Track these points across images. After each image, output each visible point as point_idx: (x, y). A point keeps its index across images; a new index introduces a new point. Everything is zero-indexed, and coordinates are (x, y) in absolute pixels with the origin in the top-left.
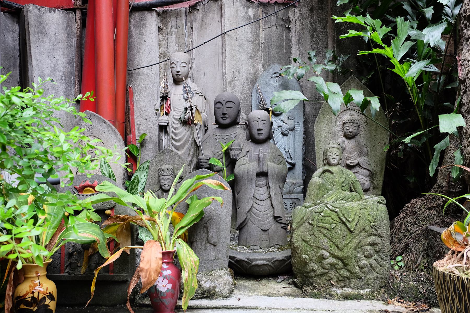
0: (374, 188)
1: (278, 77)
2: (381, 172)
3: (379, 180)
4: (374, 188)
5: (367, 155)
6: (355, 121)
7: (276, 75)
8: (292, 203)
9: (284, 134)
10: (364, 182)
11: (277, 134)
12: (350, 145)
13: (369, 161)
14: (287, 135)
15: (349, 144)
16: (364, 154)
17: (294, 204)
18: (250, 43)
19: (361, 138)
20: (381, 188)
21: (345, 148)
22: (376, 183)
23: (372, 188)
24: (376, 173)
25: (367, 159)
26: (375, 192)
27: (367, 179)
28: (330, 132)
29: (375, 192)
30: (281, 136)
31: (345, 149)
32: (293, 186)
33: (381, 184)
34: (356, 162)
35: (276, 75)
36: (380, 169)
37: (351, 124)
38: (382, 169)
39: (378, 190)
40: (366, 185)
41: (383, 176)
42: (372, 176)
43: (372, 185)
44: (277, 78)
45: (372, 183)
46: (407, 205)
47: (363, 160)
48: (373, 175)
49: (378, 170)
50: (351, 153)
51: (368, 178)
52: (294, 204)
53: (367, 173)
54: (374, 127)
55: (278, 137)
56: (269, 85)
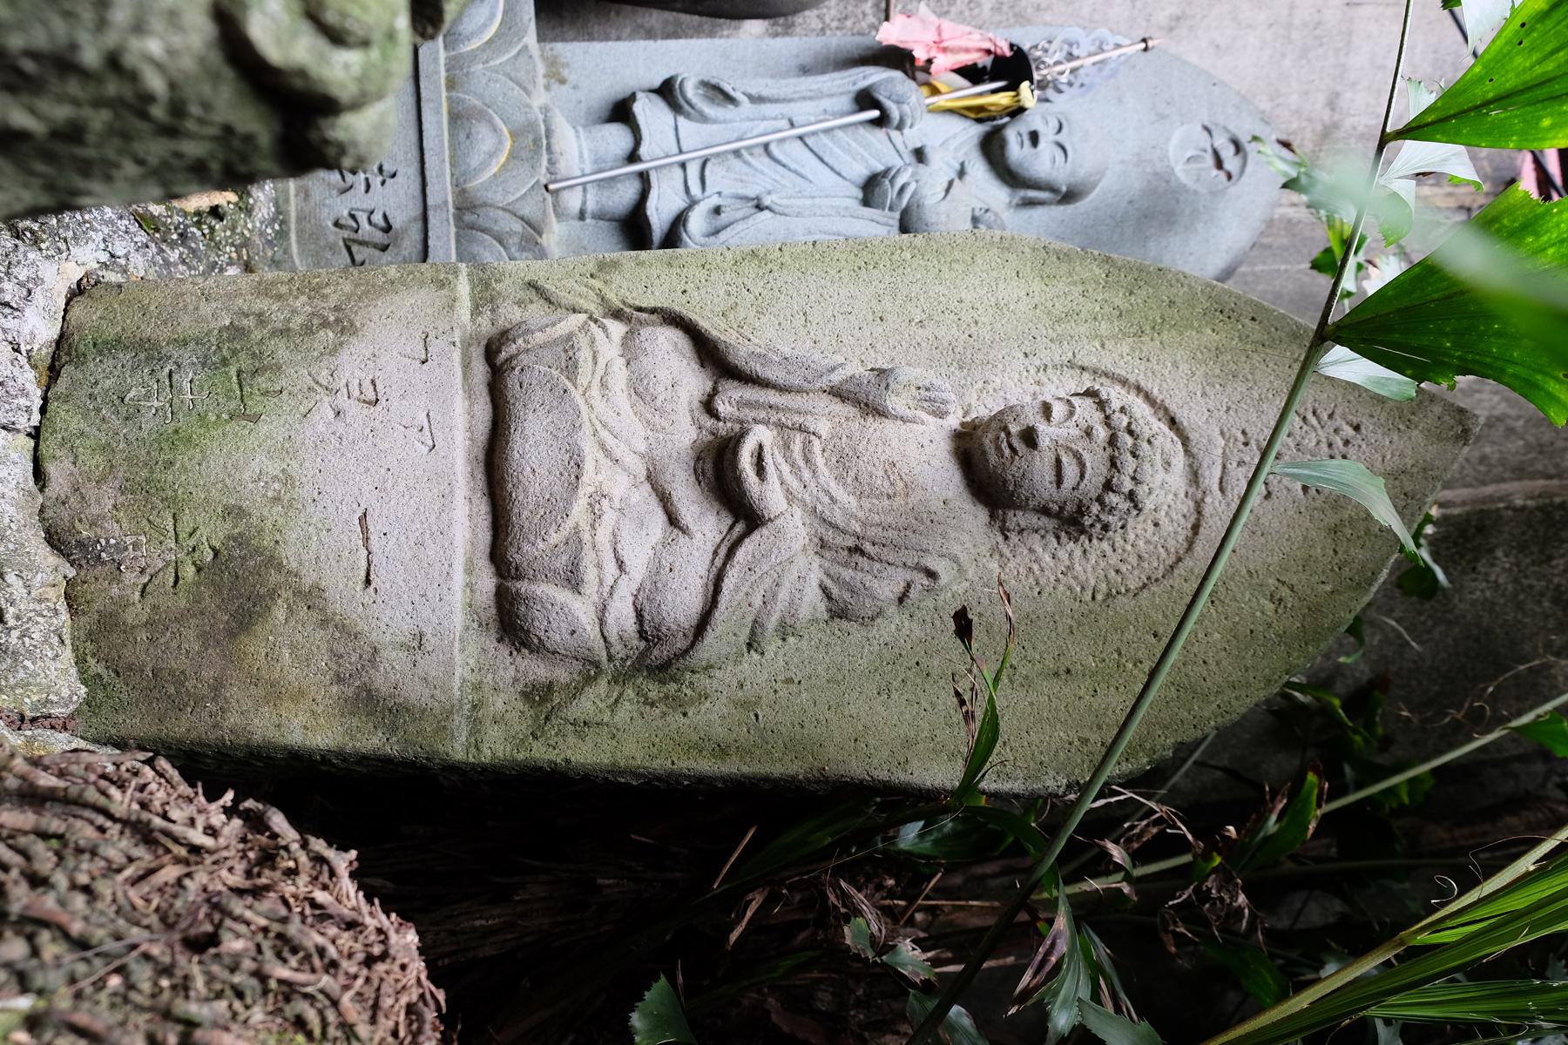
0: (538, 695)
1: (1219, 164)
2: (697, 748)
3: (618, 736)
4: (538, 695)
5: (838, 612)
6: (1129, 464)
7: (1227, 153)
8: (388, 228)
9: (871, 189)
10: (590, 575)
11: (867, 146)
12: (912, 450)
13: (785, 630)
14: (866, 202)
15: (919, 450)
16: (847, 574)
17: (379, 237)
18: (1326, 115)
19: (970, 555)
20: (540, 753)
21: (880, 413)
22: (589, 703)
23: (538, 670)
24: (678, 704)
25: (804, 613)
26: (498, 703)
27: (622, 615)
28: (985, 333)
29: (498, 703)
30: (861, 172)
31: (872, 409)
32: (518, 226)
33: (584, 753)
34: (770, 495)
35: (1227, 153)
36: (719, 732)
37: (1102, 433)
38: (722, 751)
39: (522, 728)
40: (562, 595)
41: (660, 765)
42: (658, 657)
43: (562, 675)
44: (1209, 160)
45: (590, 670)
46: (343, 861)
47: (788, 564)
48: (663, 670)
49: (712, 716)
50: (842, 461)
51: (630, 624)
52: (379, 237)
53: (683, 603)
54: (1081, 654)
55: (847, 150)
56: (1162, 117)
